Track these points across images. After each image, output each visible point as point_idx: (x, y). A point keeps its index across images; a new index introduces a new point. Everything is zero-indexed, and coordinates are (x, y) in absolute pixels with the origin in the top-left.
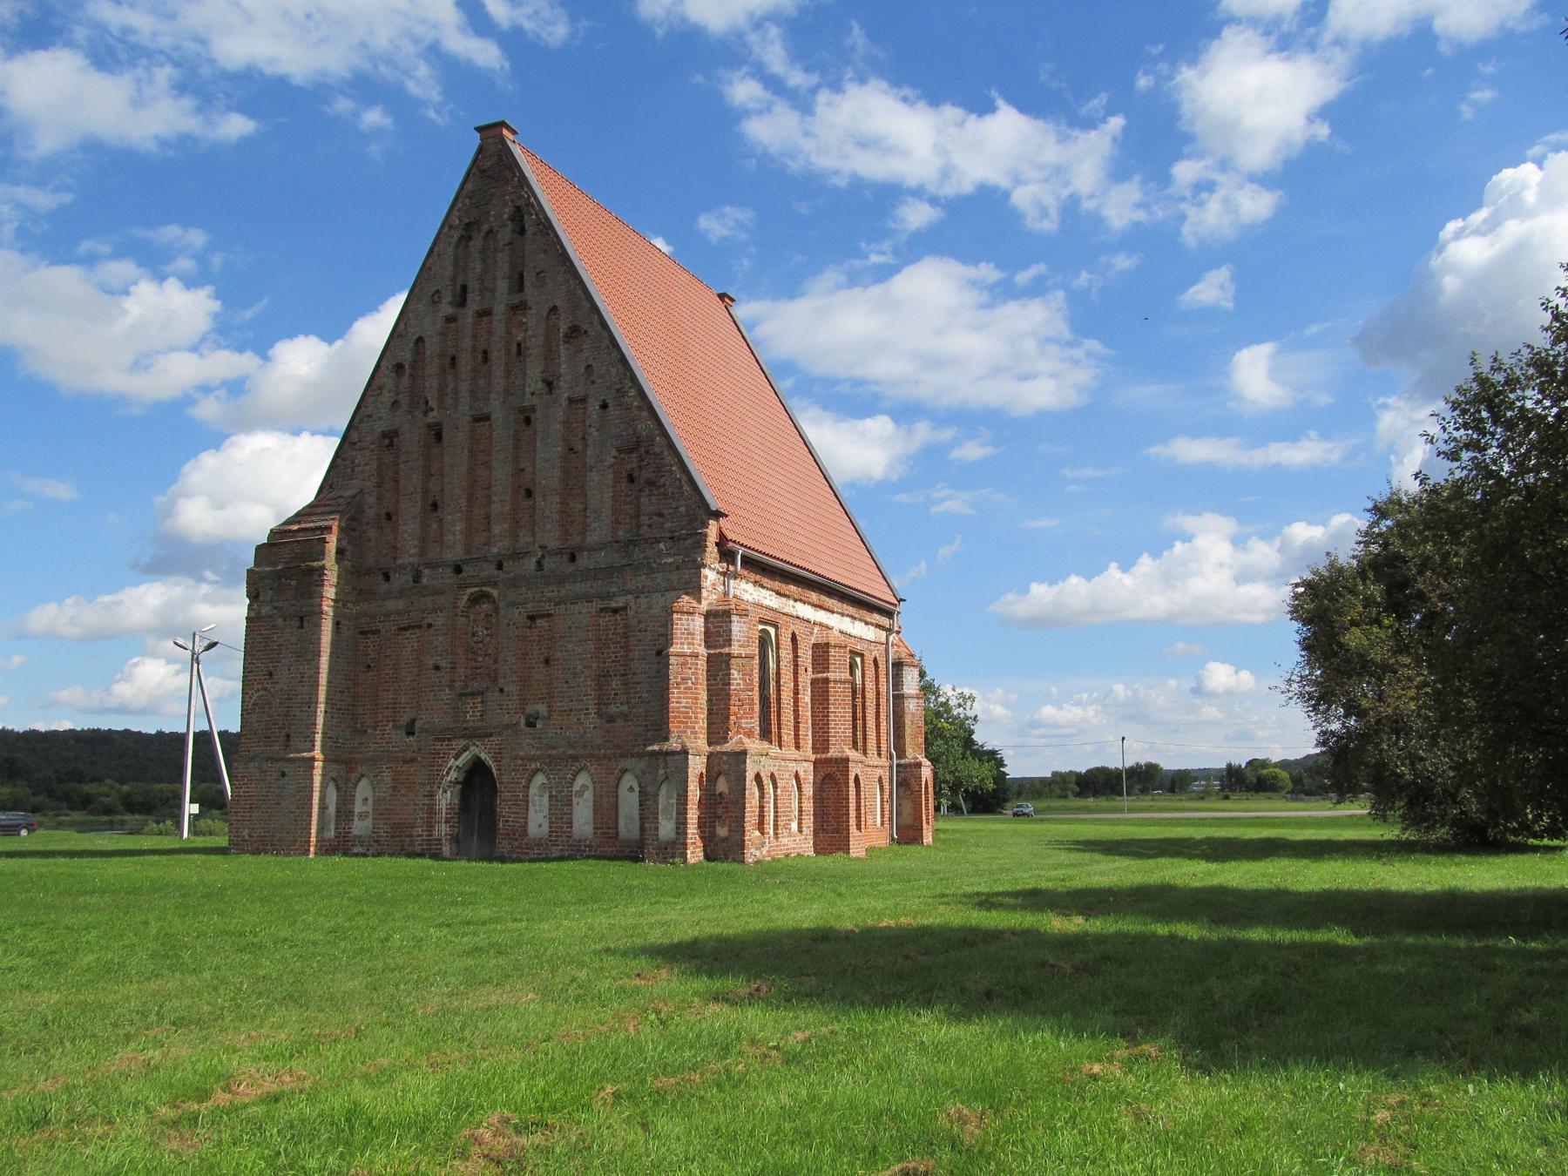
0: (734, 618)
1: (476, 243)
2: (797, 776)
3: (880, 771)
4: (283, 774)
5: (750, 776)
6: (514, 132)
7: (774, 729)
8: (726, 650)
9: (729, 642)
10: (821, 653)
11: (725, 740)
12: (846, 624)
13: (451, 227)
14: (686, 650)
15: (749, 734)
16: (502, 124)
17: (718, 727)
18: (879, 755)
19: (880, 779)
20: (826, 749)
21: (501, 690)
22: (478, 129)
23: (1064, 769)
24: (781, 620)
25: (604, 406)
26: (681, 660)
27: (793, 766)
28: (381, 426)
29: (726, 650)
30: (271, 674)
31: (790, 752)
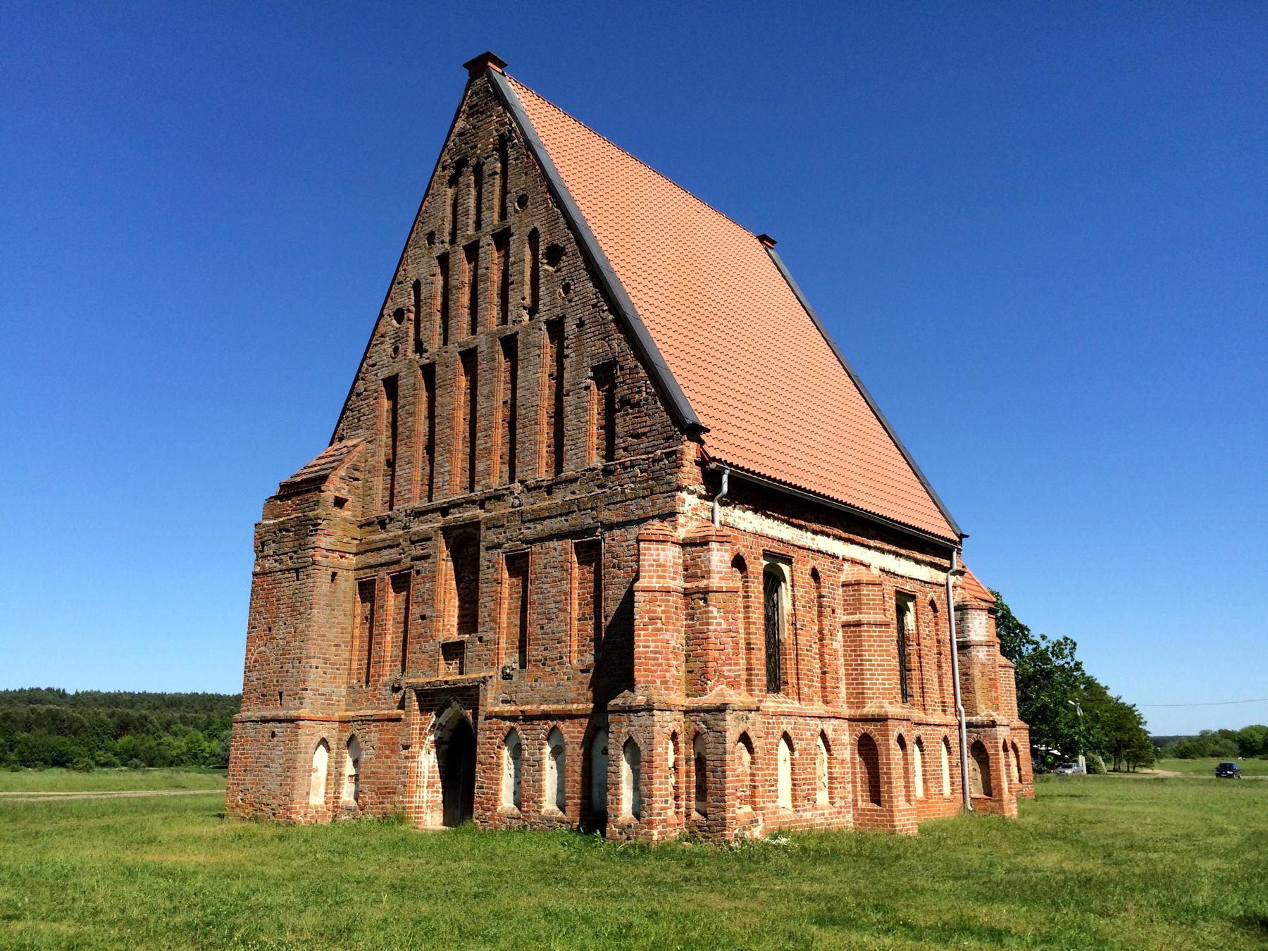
0: (714, 546)
1: (469, 178)
2: (823, 735)
3: (944, 731)
4: (273, 735)
5: (732, 735)
6: (502, 65)
7: (916, 689)
8: (703, 583)
9: (707, 574)
10: (903, 600)
11: (704, 691)
12: (890, 562)
13: (444, 168)
14: (655, 584)
15: (733, 684)
16: (489, 57)
17: (698, 679)
18: (944, 711)
19: (946, 740)
20: (861, 705)
21: (480, 639)
22: (465, 66)
23: (1214, 727)
24: (796, 554)
25: (581, 324)
26: (648, 596)
27: (818, 725)
28: (384, 373)
29: (703, 583)
30: (270, 629)
31: (819, 708)
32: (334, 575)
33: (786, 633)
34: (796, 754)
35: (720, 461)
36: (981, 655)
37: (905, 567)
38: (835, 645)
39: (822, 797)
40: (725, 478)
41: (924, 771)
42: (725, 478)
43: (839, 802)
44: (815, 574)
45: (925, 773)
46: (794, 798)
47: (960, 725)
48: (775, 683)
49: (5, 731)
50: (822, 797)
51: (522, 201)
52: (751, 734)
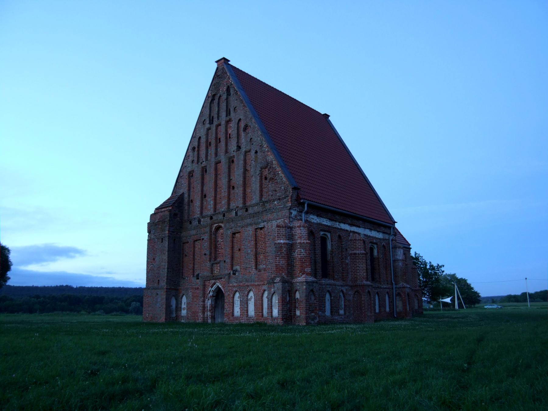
4: (157, 294)
12: (368, 232)
32: (175, 240)
33: (329, 257)
34: (332, 298)
35: (304, 199)
36: (400, 264)
37: (374, 234)
38: (347, 261)
39: (342, 312)
40: (306, 205)
41: (332, 245)
42: (306, 205)
43: (347, 314)
44: (340, 237)
45: (379, 305)
46: (331, 312)
47: (393, 289)
48: (325, 275)
49: (96, 409)
50: (342, 312)
51: (246, 128)
52: (315, 290)
